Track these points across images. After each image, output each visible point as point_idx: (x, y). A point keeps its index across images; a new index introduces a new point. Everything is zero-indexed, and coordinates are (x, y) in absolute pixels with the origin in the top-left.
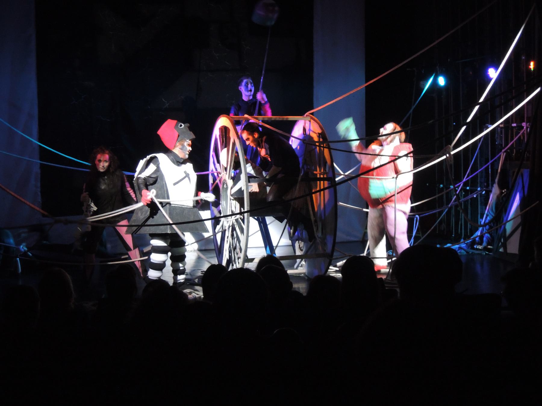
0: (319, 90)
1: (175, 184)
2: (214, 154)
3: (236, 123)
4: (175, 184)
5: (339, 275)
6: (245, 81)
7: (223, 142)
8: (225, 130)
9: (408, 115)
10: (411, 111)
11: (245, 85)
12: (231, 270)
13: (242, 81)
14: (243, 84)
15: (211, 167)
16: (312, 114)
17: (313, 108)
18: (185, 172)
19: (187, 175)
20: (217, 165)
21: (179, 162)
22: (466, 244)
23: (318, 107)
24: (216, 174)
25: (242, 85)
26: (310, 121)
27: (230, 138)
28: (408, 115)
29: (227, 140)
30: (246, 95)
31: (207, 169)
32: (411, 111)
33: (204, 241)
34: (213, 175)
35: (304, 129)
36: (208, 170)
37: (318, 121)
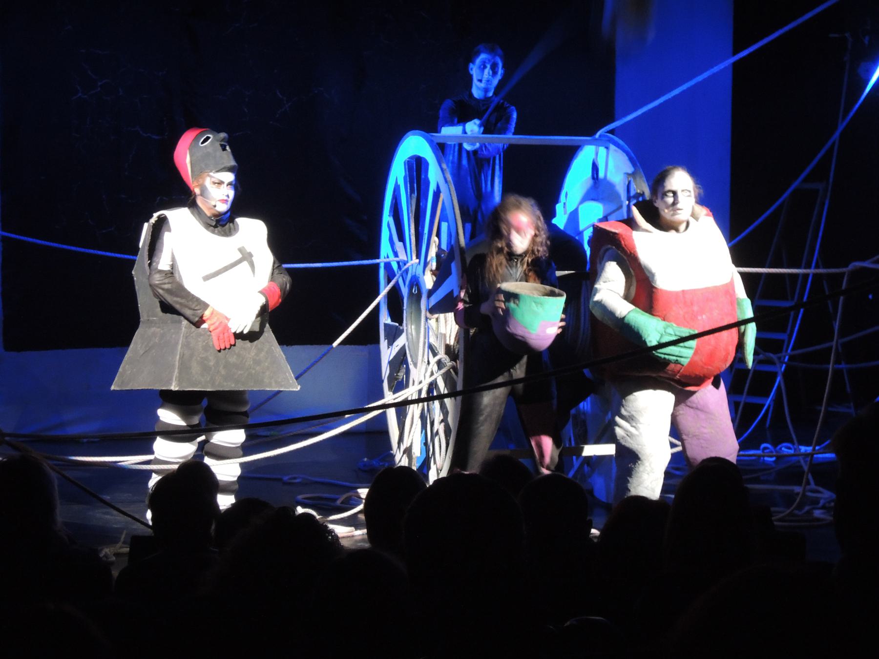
0: (625, 78)
1: (207, 278)
2: (391, 220)
3: (441, 149)
4: (207, 278)
5: (361, 533)
6: (483, 56)
7: (412, 191)
8: (417, 166)
9: (829, 143)
10: (837, 134)
11: (480, 67)
12: (435, 482)
13: (478, 54)
14: (478, 61)
15: (385, 248)
16: (611, 132)
17: (613, 120)
18: (241, 250)
19: (246, 257)
20: (399, 245)
21: (222, 223)
22: (611, 438)
23: (625, 115)
24: (395, 266)
25: (474, 63)
26: (607, 148)
27: (428, 183)
28: (829, 143)
29: (422, 187)
30: (478, 88)
31: (375, 252)
32: (837, 134)
33: (250, 421)
34: (388, 266)
35: (595, 168)
36: (378, 257)
37: (626, 147)
